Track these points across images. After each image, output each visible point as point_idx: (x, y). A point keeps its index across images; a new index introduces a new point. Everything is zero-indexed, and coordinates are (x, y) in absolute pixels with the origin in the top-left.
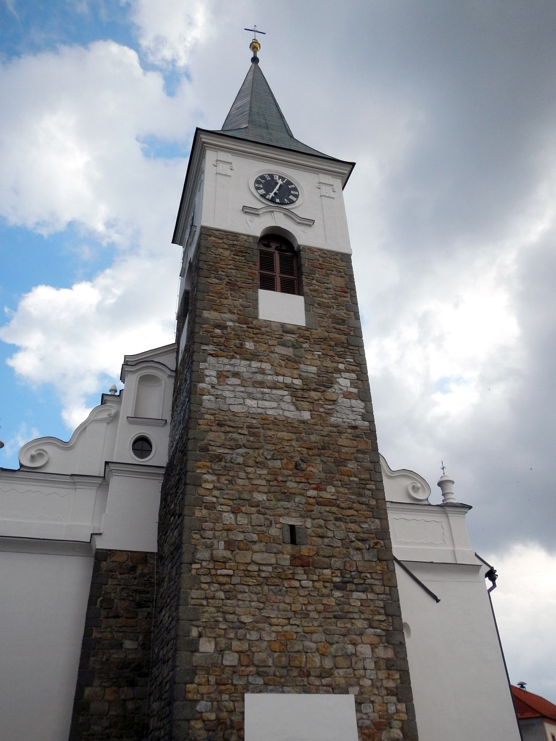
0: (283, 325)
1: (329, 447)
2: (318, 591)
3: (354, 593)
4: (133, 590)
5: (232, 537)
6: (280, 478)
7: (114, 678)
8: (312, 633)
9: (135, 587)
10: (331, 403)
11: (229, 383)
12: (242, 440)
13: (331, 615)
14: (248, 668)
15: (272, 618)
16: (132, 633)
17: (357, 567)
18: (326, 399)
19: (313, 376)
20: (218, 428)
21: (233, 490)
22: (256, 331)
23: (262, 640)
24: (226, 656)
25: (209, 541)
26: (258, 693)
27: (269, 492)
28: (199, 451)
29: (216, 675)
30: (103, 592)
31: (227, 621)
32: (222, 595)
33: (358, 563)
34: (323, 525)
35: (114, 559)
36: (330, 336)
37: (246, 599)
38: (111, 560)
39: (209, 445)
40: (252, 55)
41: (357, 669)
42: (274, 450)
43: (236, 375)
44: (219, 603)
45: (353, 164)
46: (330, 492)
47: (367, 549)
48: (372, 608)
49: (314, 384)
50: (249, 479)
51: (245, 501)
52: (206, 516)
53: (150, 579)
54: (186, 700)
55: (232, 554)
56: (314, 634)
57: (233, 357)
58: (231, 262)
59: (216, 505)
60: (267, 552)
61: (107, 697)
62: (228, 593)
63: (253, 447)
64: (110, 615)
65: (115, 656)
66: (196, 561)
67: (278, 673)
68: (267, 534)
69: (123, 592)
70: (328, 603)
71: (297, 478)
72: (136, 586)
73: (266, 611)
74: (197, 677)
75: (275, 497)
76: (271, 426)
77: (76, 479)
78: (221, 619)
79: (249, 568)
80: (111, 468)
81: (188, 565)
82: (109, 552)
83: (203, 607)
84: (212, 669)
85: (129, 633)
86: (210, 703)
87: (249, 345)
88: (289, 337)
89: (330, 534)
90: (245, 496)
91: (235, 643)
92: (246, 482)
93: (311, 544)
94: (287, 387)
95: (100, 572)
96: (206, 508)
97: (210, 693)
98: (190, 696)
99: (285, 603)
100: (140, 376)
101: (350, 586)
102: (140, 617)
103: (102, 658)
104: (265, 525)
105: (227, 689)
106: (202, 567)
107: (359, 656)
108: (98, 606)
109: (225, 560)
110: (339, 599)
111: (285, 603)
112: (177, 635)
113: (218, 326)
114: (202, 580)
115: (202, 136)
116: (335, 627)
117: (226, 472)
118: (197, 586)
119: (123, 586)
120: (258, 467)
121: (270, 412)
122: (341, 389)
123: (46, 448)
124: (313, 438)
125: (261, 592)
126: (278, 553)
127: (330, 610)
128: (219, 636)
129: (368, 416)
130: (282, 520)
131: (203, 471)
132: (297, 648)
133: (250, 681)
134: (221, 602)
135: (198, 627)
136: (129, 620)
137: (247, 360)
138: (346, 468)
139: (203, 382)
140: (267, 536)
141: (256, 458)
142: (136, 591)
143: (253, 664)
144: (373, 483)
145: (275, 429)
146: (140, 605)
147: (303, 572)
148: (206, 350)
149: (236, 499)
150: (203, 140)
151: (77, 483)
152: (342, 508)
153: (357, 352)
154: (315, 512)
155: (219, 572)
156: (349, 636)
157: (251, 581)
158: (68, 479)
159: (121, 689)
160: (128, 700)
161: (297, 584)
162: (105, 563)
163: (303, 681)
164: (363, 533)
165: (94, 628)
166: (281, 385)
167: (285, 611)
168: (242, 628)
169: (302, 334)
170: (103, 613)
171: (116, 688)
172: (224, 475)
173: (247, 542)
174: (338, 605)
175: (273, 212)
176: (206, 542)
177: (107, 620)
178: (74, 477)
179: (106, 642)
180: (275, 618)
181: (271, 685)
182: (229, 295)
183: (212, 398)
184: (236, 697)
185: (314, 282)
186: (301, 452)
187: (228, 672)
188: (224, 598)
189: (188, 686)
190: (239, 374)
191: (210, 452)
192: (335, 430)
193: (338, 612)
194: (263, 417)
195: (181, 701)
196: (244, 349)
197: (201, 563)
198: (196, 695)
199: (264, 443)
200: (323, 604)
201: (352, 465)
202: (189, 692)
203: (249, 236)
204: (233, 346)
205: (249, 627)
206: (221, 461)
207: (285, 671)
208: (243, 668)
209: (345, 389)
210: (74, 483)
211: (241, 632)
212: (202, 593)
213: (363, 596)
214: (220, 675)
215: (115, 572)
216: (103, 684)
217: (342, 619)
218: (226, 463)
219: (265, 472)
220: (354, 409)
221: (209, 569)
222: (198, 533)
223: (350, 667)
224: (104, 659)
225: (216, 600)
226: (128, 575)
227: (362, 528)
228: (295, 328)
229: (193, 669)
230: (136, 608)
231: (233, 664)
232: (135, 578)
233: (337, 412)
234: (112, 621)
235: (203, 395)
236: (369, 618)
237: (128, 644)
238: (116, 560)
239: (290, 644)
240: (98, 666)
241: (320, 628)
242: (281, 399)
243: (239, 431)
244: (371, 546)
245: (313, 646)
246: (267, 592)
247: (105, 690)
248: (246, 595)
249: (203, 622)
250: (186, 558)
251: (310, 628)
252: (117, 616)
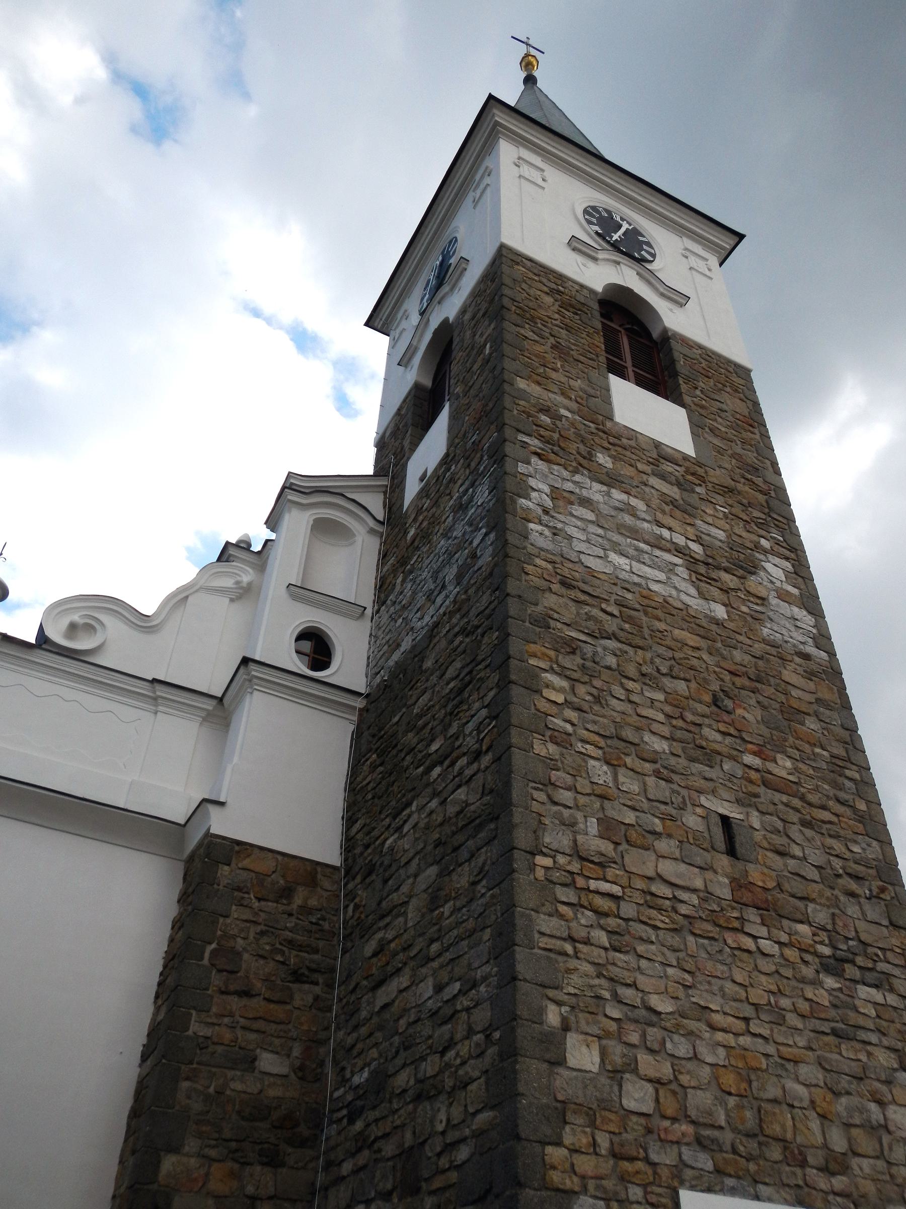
0: (657, 445)
1: (768, 681)
2: (794, 969)
3: (858, 986)
4: (285, 940)
5: (611, 813)
6: (690, 717)
7: (231, 1140)
8: (796, 1062)
9: (288, 933)
10: (759, 601)
11: (575, 513)
12: (611, 625)
13: (826, 1027)
14: (676, 1126)
15: (712, 1011)
16: (278, 1037)
17: (857, 932)
18: (748, 592)
19: (720, 544)
20: (563, 591)
21: (604, 716)
22: (612, 440)
23: (699, 1060)
24: (627, 1087)
25: (566, 813)
26: (703, 1191)
27: (674, 740)
28: (531, 623)
29: (610, 1132)
30: (219, 933)
31: (620, 1002)
32: (602, 938)
33: (857, 922)
34: (781, 829)
35: (246, 863)
36: (739, 488)
37: (654, 957)
38: (240, 865)
39: (550, 617)
40: (523, 75)
41: (896, 1165)
42: (670, 659)
43: (586, 502)
44: (600, 956)
45: (741, 237)
46: (783, 766)
47: (867, 898)
48: (898, 1026)
49: (724, 560)
50: (630, 702)
51: (628, 745)
52: (557, 757)
53: (321, 922)
54: (547, 1189)
55: (615, 849)
56: (801, 1065)
57: (575, 472)
58: (557, 316)
59: (573, 739)
60: (684, 862)
61: (214, 1185)
62: (615, 937)
63: (633, 644)
64: (232, 988)
65: (238, 1086)
66: (544, 850)
67: (742, 1148)
68: (679, 823)
69: (265, 940)
70: (815, 999)
71: (719, 724)
72: (291, 931)
73: (699, 992)
74: (568, 1128)
75: (684, 749)
76: (659, 613)
77: (161, 691)
78: (607, 995)
79: (653, 889)
80: (254, 673)
81: (529, 856)
82: (237, 848)
83: (565, 958)
84: (601, 1116)
85: (272, 1035)
86: (602, 1203)
87: (602, 459)
88: (668, 467)
89: (797, 851)
90: (628, 733)
91: (643, 1058)
92: (628, 708)
93: (765, 865)
94: (679, 551)
95: (215, 886)
96: (553, 740)
97: (601, 1178)
98: (555, 1177)
99: (734, 982)
100: (315, 517)
101: (851, 971)
102: (297, 1002)
103: (209, 1087)
104: (672, 803)
105: (637, 1172)
106: (556, 867)
107: (894, 1132)
108: (206, 961)
109: (602, 859)
110: (835, 993)
111: (734, 982)
112: (516, 1015)
113: (546, 410)
114: (558, 896)
115: (495, 111)
116: (837, 1057)
117: (586, 679)
118: (548, 908)
119: (264, 928)
120: (645, 684)
121: (655, 587)
122: (772, 582)
123: (103, 617)
124: (738, 655)
125: (682, 947)
126: (707, 869)
127: (823, 1016)
128: (608, 1035)
129: (823, 639)
130: (703, 800)
131: (542, 665)
132: (772, 1092)
133: (685, 1157)
134: (603, 952)
135: (559, 1003)
136: (272, 1006)
137: (602, 483)
138: (804, 728)
139: (528, 497)
140: (679, 826)
141: (641, 665)
142: (290, 943)
143: (687, 1116)
144: (854, 767)
145: (668, 621)
146: (297, 977)
147: (759, 921)
148: (527, 443)
149: (611, 738)
150: (497, 118)
151: (160, 701)
152: (810, 804)
153: (786, 527)
154: (762, 800)
155: (593, 884)
156: (868, 1081)
157: (659, 919)
158: (143, 688)
159: (248, 1169)
160: (261, 1199)
161: (749, 943)
162: (226, 868)
163: (794, 1174)
164: (856, 863)
165: (194, 1013)
166: (668, 545)
167: (735, 1000)
168: (653, 1026)
169: (692, 470)
170: (217, 980)
171: (236, 1166)
172: (583, 683)
173: (644, 833)
174: (835, 1006)
175: (618, 263)
176: (561, 814)
177: (224, 997)
178: (158, 687)
179: (220, 1049)
180: (718, 1011)
181: (730, 1176)
182: (559, 366)
183: (547, 532)
184: (660, 1195)
185: (698, 392)
186: (721, 676)
187: (636, 1127)
188: (608, 945)
189: (549, 1149)
190: (591, 504)
191: (551, 630)
192: (773, 651)
193: (837, 1022)
194: (645, 592)
195: (535, 1189)
196: (595, 464)
197: (554, 857)
198: (570, 1177)
199: (650, 641)
200: (807, 999)
201: (812, 724)
202: (554, 1168)
203: (582, 286)
204: (575, 452)
205: (668, 1025)
206: (573, 652)
207: (753, 1145)
208: (667, 1123)
209: (778, 584)
210: (155, 699)
211: (653, 1033)
212: (562, 926)
213: (877, 995)
214: (620, 1133)
215: (248, 893)
216: (207, 1151)
217: (849, 1039)
218: (584, 659)
219: (660, 696)
220: (799, 624)
221: (571, 873)
222: (541, 790)
223: (880, 1156)
224: (211, 1090)
225: (593, 947)
226: (275, 905)
227: (851, 851)
228: (679, 456)
229: (556, 1108)
230: (289, 982)
231: (644, 1110)
232: (290, 915)
233: (771, 620)
234: (235, 1003)
235: (529, 521)
236: (896, 1048)
237: (269, 1062)
238: (251, 867)
239: (758, 1080)
240: (197, 1106)
241: (810, 1053)
242: (670, 569)
243: (604, 606)
244: (875, 893)
245: (802, 1090)
246: (695, 950)
247: (210, 1167)
248: (653, 947)
249: (569, 994)
250: (522, 838)
251: (790, 1050)
252: (246, 993)
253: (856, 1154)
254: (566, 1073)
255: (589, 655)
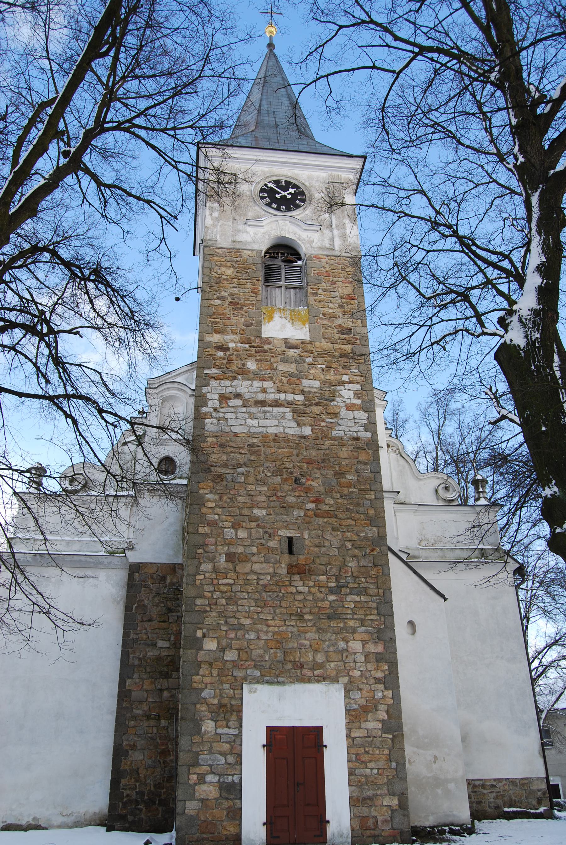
64: (144, 619)
69: (156, 599)
96: (208, 525)
101: (344, 590)
131: (206, 491)
189: (194, 677)
197: (204, 575)
211: (240, 633)
224: (141, 656)
234: (146, 624)
243: (240, 451)
253: (329, 661)
254: (202, 652)
255: (229, 480)
